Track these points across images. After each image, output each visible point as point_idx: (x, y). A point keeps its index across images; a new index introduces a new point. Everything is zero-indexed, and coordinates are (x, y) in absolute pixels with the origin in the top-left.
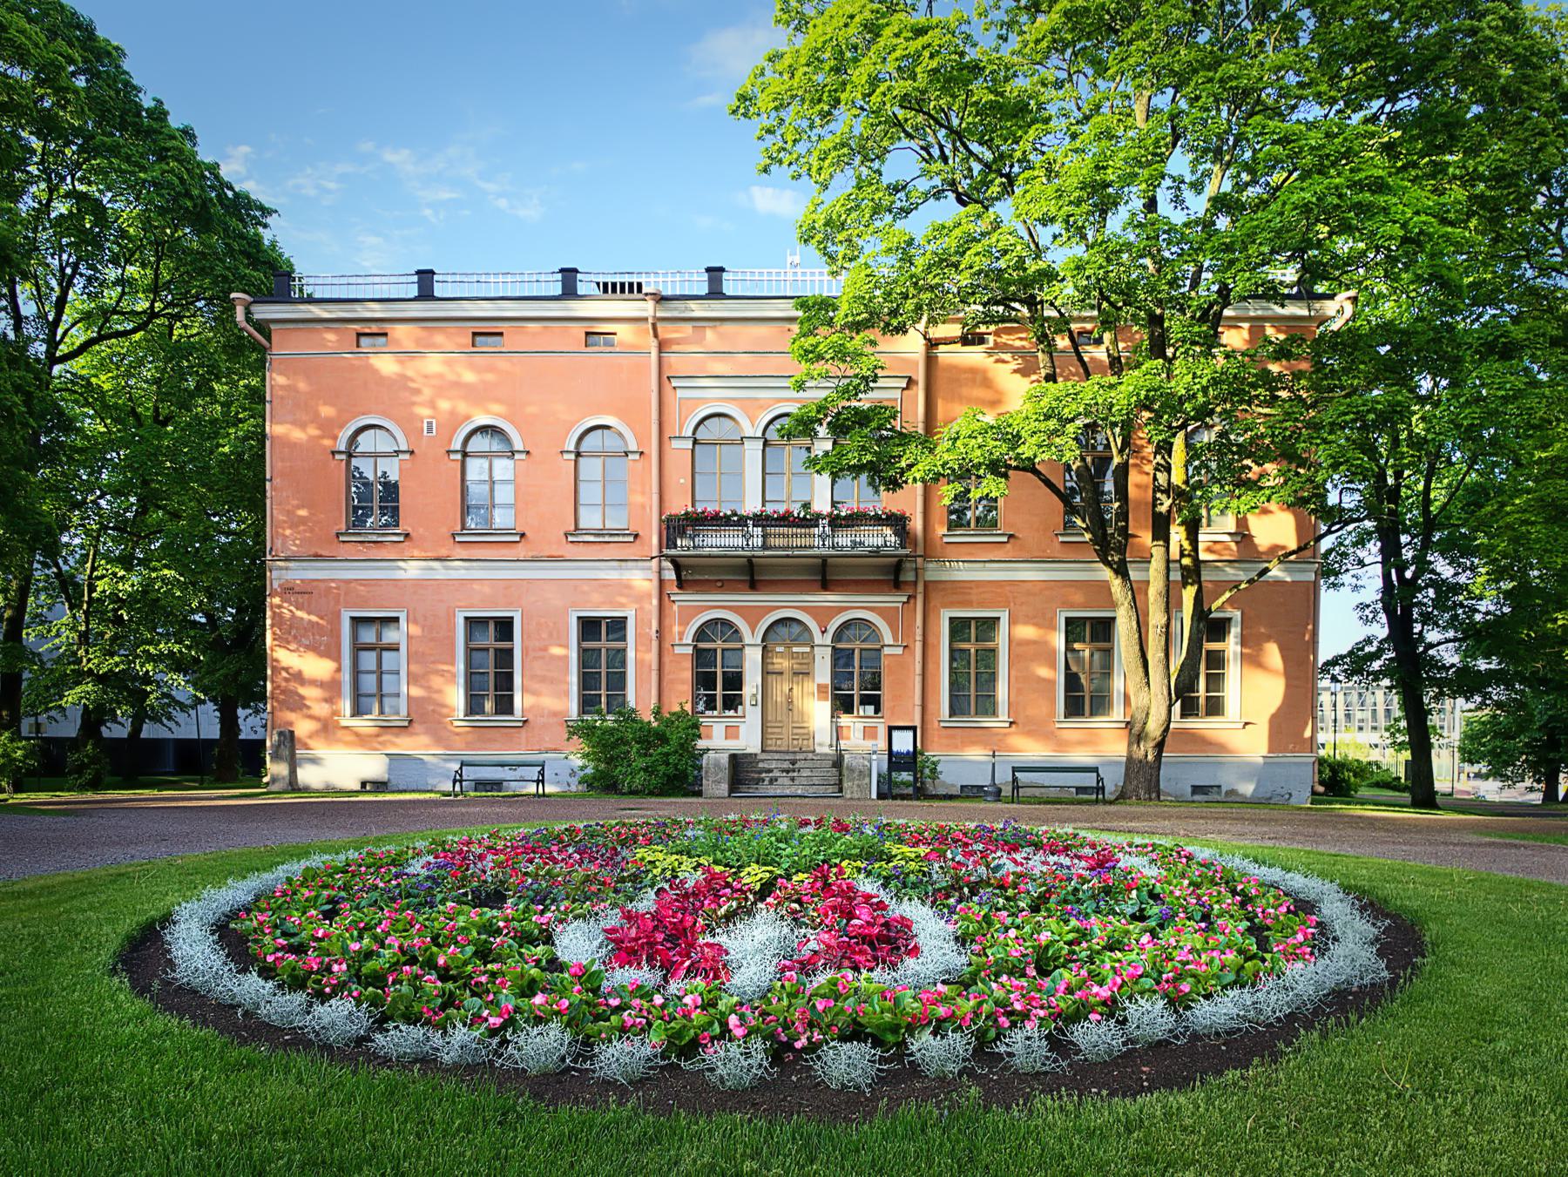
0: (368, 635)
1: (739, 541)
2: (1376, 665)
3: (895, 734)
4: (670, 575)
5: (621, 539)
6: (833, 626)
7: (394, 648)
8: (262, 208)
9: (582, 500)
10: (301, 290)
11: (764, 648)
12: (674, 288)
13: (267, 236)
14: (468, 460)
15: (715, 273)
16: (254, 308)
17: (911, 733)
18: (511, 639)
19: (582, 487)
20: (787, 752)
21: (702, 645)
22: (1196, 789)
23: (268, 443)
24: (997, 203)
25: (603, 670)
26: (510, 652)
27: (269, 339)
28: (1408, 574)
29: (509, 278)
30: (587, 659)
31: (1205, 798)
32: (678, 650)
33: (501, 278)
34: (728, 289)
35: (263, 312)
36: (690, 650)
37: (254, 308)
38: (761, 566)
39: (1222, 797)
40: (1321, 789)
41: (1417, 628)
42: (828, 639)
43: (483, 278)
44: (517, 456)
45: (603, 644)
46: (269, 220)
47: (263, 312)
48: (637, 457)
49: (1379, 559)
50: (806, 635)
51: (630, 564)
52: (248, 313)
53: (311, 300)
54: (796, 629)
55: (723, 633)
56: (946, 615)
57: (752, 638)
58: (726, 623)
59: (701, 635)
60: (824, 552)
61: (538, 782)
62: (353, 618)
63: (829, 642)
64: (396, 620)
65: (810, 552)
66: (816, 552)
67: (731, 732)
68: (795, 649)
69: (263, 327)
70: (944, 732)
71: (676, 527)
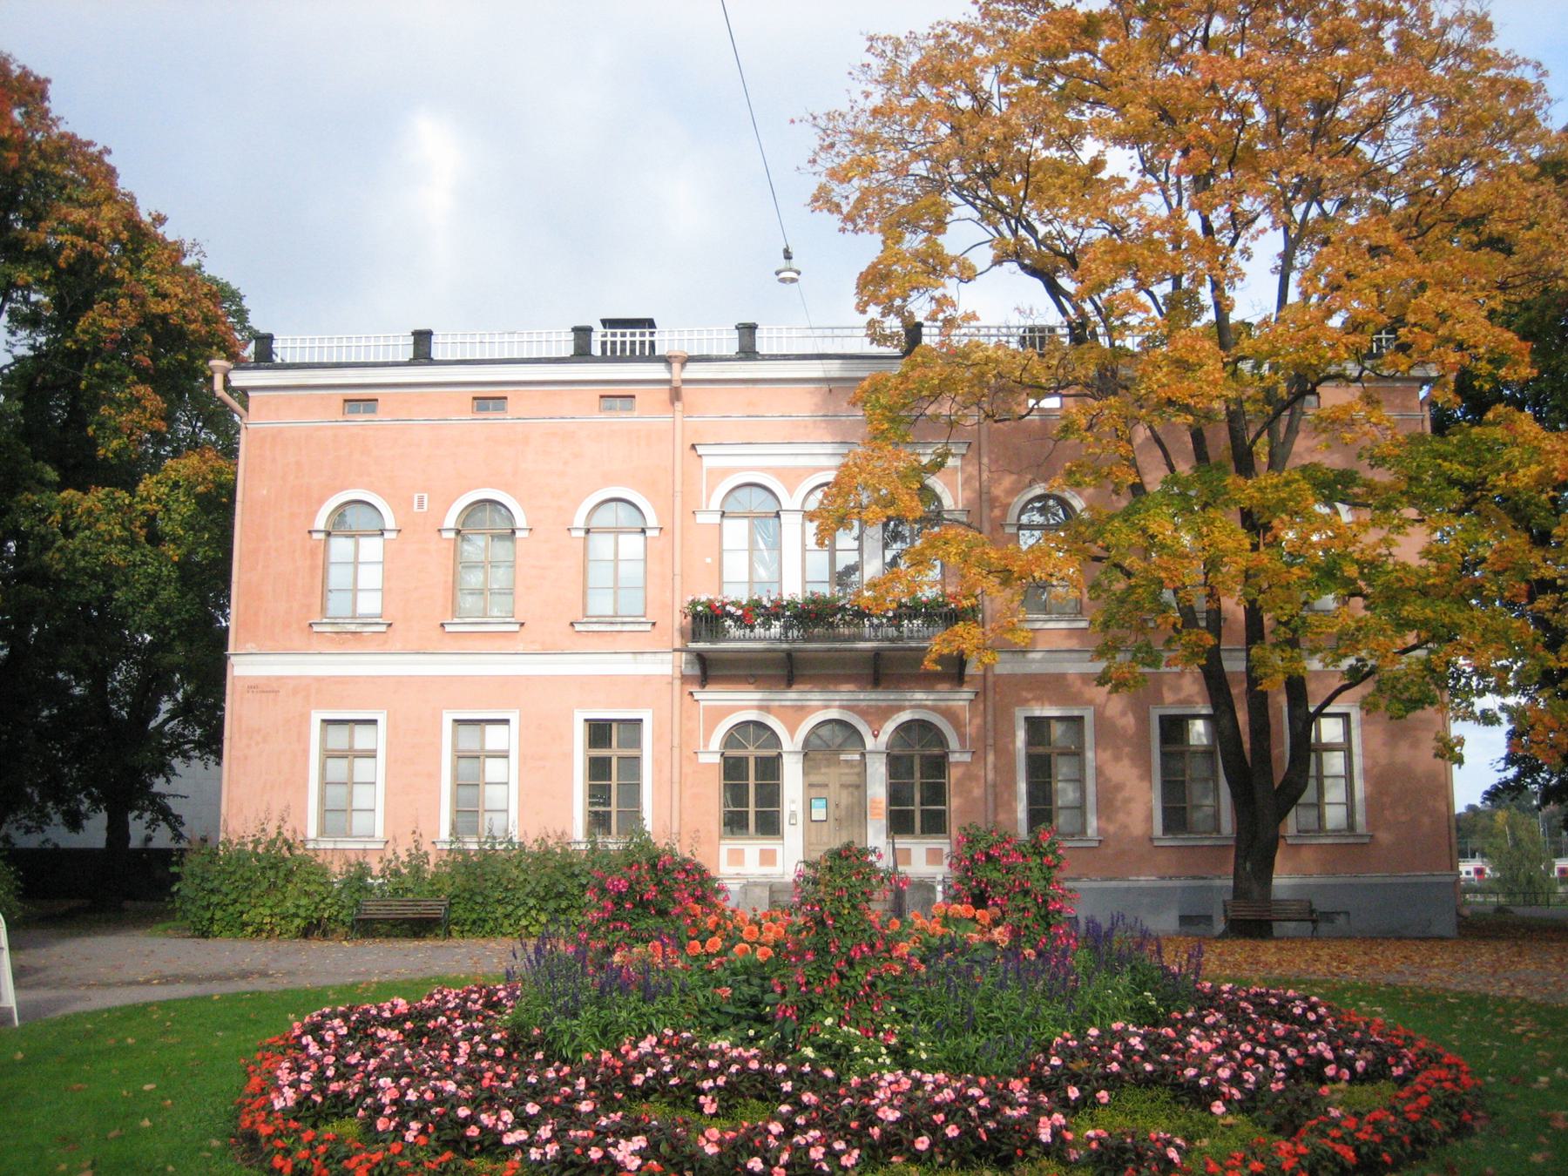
0: (338, 739)
6: (890, 727)
7: (371, 754)
9: (591, 584)
11: (805, 755)
12: (311, 354)
14: (593, 537)
15: (748, 331)
19: (592, 567)
24: (1281, 248)
30: (598, 768)
32: (703, 758)
34: (762, 347)
35: (239, 379)
36: (717, 759)
37: (232, 376)
44: (387, 535)
47: (239, 379)
48: (656, 533)
50: (815, 741)
51: (646, 657)
52: (226, 380)
53: (765, 358)
55: (757, 739)
57: (791, 744)
59: (730, 740)
67: (767, 858)
69: (243, 394)
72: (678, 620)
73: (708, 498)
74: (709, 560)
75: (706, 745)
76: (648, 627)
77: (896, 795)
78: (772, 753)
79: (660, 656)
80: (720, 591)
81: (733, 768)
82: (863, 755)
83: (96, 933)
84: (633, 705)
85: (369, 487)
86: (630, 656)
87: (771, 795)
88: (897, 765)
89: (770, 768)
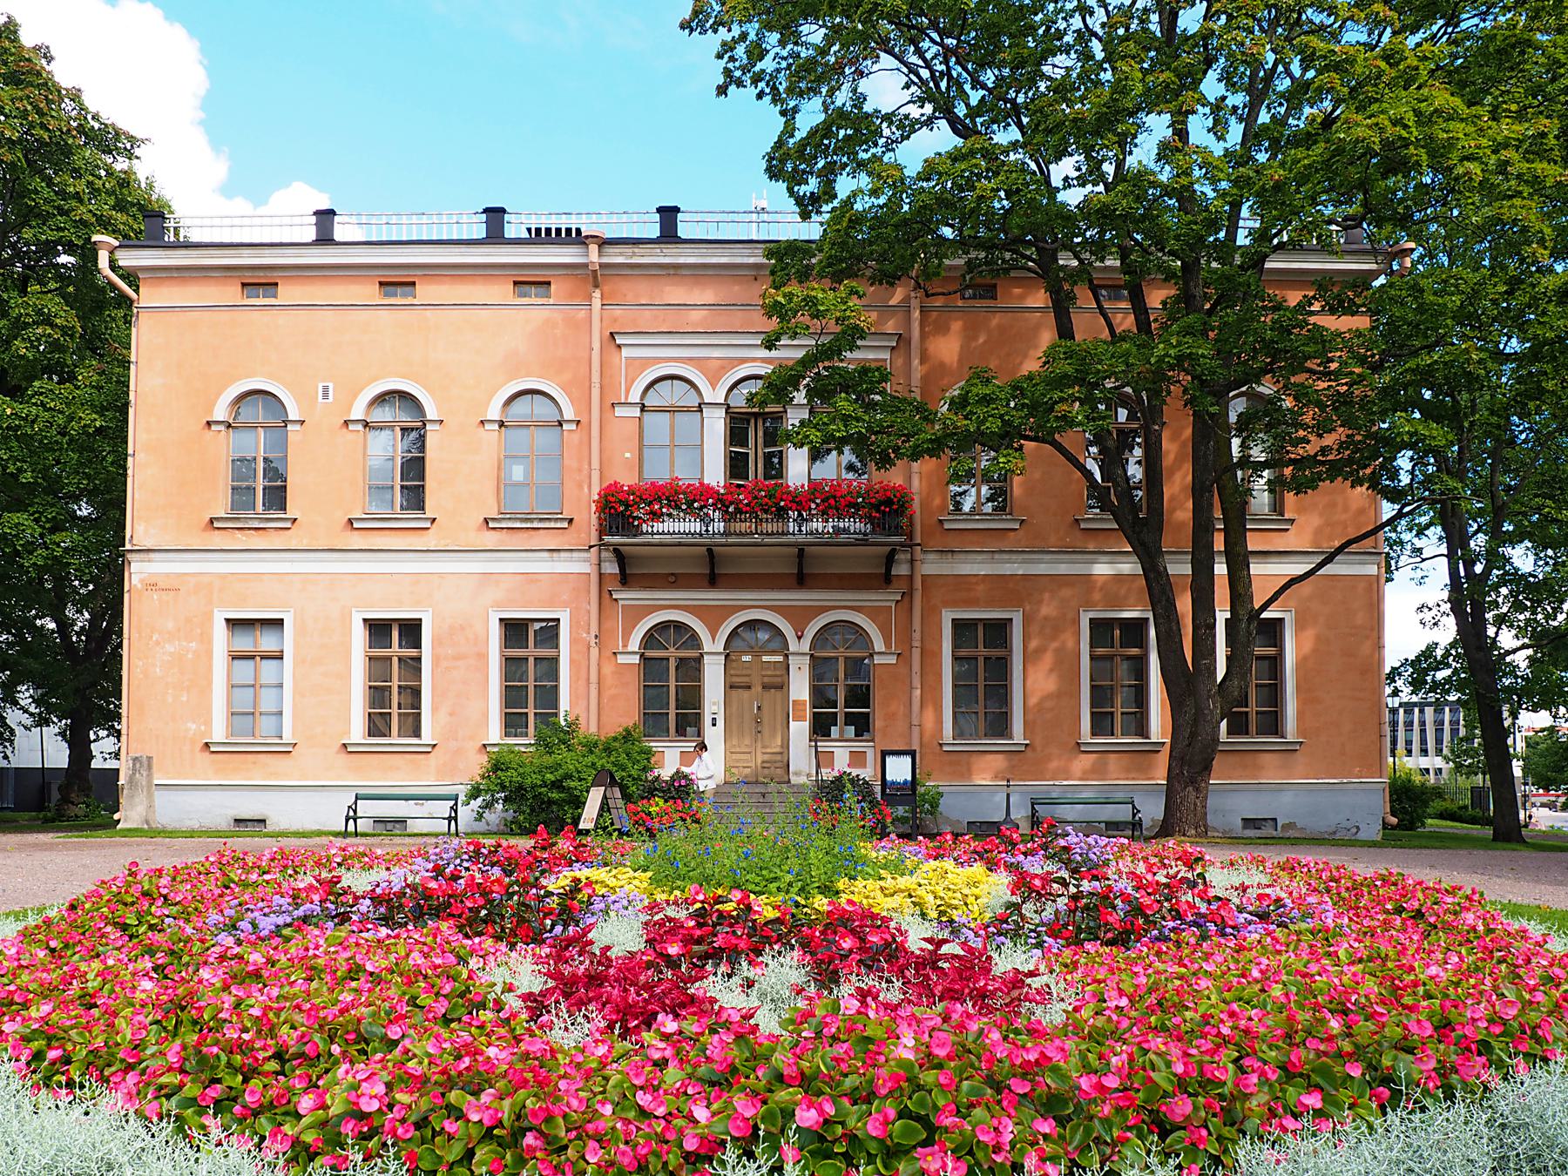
1: (696, 526)
2: (1441, 675)
3: (890, 760)
4: (611, 568)
5: (552, 525)
6: (811, 631)
8: (131, 138)
10: (176, 234)
11: (727, 656)
13: (142, 170)
15: (668, 214)
16: (119, 254)
17: (908, 759)
18: (418, 646)
20: (757, 782)
21: (650, 653)
22: (1248, 823)
23: (131, 411)
25: (531, 684)
26: (555, 661)
27: (137, 291)
28: (1479, 568)
29: (424, 219)
30: (512, 666)
31: (1257, 833)
32: (621, 659)
33: (415, 219)
35: (127, 259)
36: (636, 659)
37: (119, 254)
38: (633, 557)
39: (1279, 833)
40: (1394, 820)
41: (1491, 631)
42: (805, 646)
43: (394, 220)
45: (531, 651)
46: (137, 152)
47: (127, 259)
48: (573, 427)
49: (1444, 549)
51: (563, 554)
54: (763, 636)
56: (948, 616)
57: (712, 645)
58: (679, 627)
59: (649, 640)
60: (800, 539)
61: (449, 819)
62: (228, 620)
63: (807, 650)
64: (279, 623)
65: (783, 539)
66: (791, 539)
68: (765, 659)
69: (131, 277)
70: (947, 758)
71: (619, 512)
72: (588, 519)
73: (627, 392)
74: (628, 455)
75: (625, 646)
76: (565, 525)
77: (820, 695)
78: (693, 654)
79: (575, 554)
80: (672, 471)
81: (650, 667)
82: (786, 656)
83: (1517, 880)
84: (551, 603)
85: (271, 376)
86: (546, 554)
87: (691, 699)
88: (819, 667)
89: (692, 668)
